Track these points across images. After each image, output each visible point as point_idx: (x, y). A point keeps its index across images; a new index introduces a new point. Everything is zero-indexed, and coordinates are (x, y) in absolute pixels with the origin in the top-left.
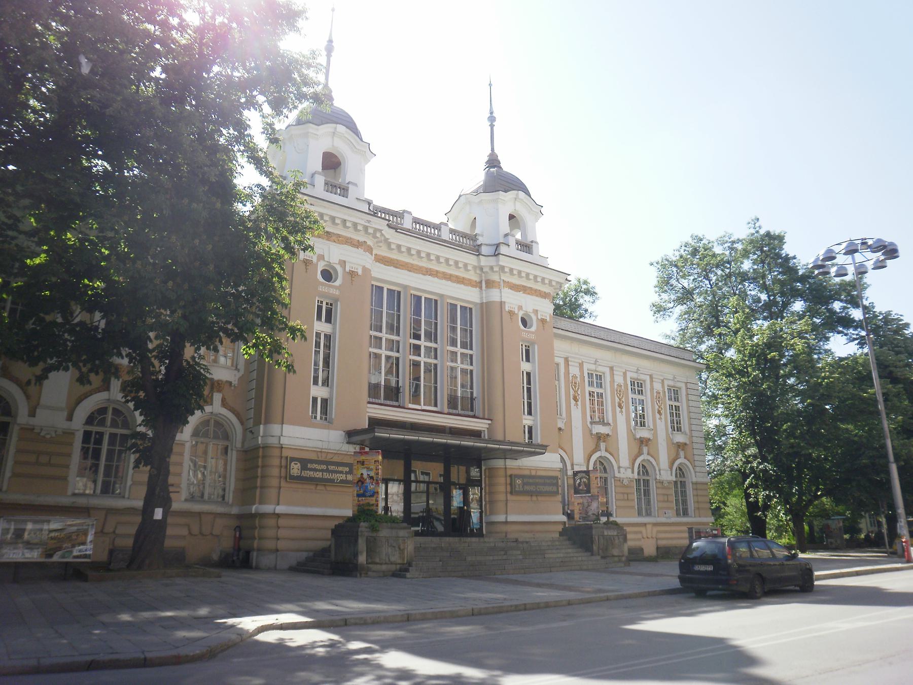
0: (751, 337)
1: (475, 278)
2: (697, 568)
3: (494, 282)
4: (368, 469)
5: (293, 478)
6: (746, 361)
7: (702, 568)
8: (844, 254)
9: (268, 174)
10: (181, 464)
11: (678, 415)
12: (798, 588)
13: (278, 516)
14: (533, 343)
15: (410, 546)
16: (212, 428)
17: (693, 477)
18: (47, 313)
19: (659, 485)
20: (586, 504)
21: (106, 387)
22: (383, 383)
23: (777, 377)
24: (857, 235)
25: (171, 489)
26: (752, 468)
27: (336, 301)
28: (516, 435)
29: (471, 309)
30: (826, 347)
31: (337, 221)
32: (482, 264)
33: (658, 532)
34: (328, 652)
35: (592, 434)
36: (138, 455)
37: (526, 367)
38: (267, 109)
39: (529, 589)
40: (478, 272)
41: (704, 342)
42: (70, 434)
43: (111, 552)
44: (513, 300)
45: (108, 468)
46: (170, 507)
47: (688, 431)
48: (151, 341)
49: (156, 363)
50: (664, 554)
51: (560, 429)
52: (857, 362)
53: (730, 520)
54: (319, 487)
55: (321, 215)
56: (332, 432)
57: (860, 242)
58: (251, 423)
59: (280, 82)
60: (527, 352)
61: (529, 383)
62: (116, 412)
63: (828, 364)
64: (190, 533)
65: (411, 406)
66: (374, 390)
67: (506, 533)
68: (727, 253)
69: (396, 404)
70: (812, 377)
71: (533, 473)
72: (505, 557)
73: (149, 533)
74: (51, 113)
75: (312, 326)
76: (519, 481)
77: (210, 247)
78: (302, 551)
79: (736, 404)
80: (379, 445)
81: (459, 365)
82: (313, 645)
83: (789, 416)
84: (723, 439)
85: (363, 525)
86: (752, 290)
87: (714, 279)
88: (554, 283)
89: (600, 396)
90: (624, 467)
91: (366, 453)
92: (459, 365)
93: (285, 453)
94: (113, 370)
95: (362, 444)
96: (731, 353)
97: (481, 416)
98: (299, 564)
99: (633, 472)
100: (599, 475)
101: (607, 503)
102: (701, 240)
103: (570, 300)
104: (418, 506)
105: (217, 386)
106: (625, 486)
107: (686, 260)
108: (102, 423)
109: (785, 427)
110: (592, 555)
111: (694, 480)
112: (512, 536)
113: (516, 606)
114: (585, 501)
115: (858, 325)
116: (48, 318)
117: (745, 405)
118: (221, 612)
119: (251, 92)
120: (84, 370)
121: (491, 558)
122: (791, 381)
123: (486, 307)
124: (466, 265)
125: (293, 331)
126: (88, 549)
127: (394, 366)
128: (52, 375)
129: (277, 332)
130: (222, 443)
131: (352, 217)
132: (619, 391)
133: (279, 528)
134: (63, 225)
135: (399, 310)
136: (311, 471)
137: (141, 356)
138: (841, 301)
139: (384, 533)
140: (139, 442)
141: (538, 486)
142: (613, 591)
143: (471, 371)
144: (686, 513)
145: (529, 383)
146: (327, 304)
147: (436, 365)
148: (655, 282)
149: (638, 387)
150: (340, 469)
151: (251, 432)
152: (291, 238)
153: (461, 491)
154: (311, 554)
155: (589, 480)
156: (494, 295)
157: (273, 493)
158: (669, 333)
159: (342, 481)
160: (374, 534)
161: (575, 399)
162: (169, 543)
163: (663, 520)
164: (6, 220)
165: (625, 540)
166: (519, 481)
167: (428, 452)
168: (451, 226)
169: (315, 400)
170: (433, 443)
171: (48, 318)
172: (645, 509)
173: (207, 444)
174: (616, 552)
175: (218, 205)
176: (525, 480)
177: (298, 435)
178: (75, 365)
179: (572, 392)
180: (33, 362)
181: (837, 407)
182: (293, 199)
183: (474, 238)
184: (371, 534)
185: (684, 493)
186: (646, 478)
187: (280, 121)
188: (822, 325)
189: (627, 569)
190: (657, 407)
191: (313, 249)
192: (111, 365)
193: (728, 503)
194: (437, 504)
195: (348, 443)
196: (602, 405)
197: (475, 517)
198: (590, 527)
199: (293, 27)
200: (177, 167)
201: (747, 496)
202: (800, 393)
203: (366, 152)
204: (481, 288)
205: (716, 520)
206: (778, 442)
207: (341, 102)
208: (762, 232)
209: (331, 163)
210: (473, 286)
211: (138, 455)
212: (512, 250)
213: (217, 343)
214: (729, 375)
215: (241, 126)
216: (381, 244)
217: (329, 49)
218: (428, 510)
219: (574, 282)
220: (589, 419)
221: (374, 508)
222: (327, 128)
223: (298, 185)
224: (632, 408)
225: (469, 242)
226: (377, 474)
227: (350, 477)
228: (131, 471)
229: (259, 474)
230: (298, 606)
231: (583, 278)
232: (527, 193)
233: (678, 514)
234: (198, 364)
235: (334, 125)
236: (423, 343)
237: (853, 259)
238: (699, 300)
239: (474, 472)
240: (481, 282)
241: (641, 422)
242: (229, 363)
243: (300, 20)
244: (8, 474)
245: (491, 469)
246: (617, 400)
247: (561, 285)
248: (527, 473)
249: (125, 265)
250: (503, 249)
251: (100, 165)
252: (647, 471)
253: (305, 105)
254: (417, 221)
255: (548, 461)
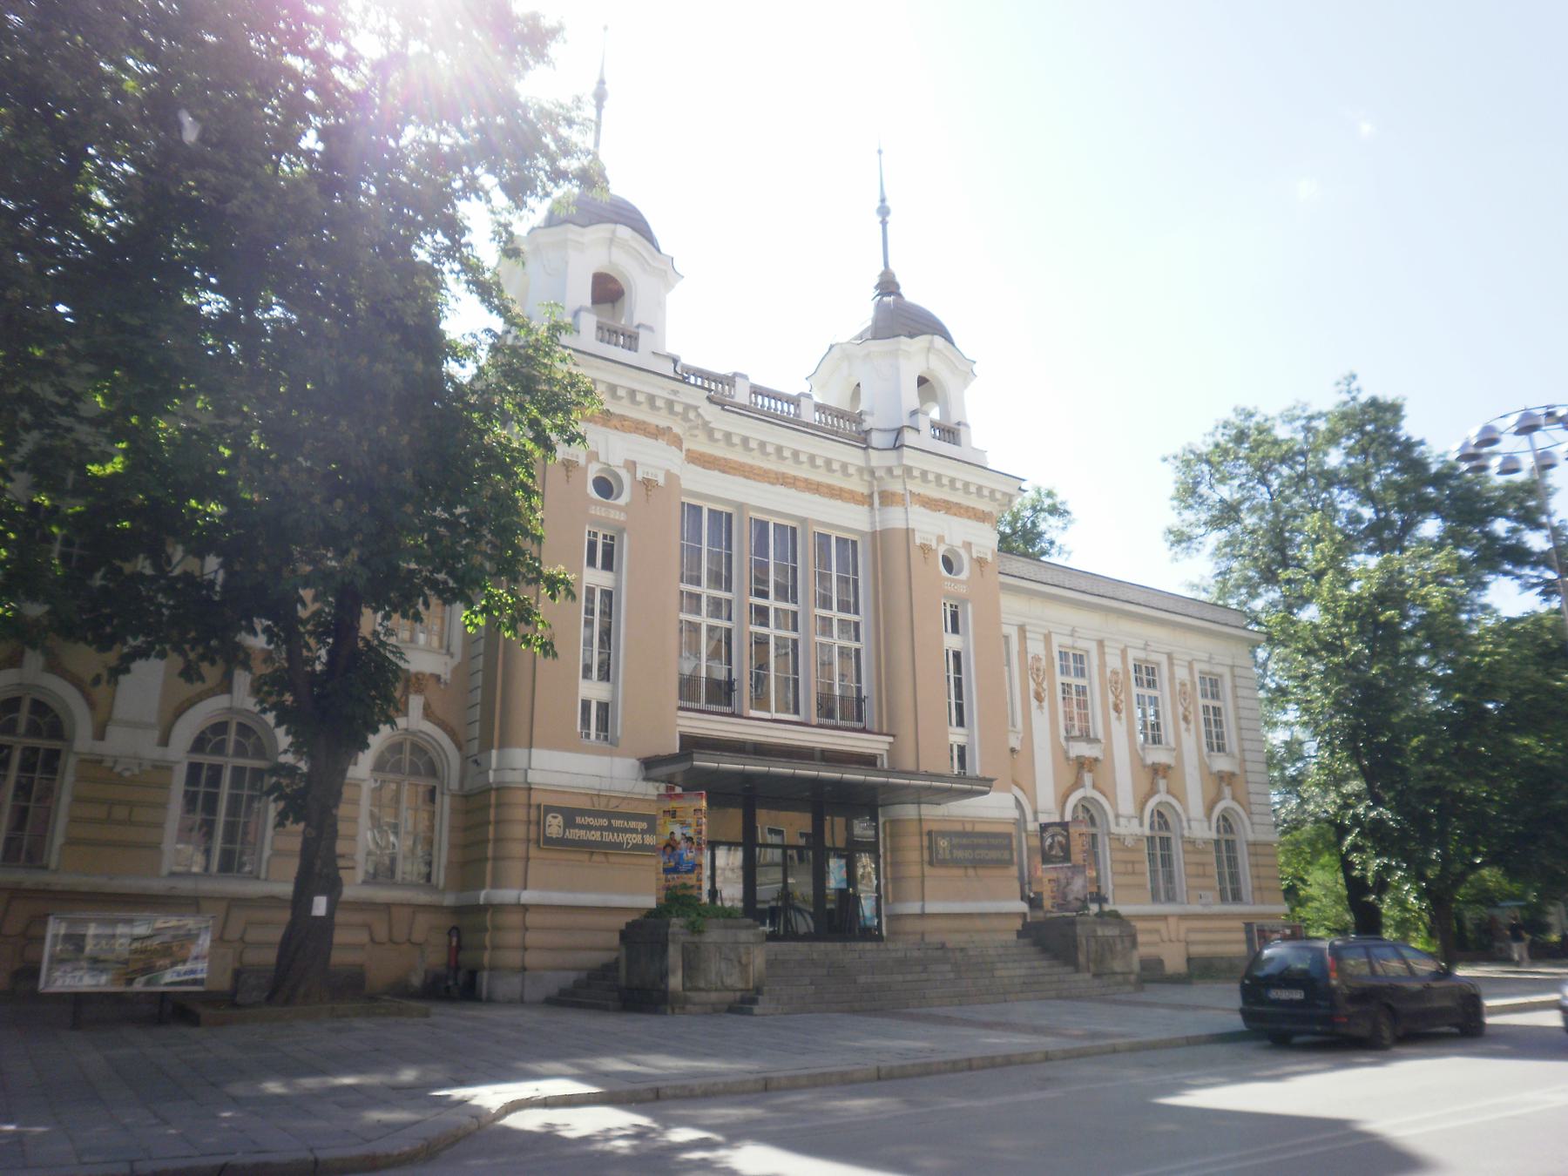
0: (1347, 585)
1: (861, 488)
2: (1275, 994)
3: (893, 494)
4: (683, 824)
5: (552, 842)
6: (1339, 627)
7: (1284, 995)
8: (1518, 433)
9: (503, 311)
10: (354, 820)
11: (1218, 723)
12: (1455, 1030)
13: (525, 908)
14: (964, 601)
15: (758, 959)
16: (407, 756)
17: (1247, 832)
18: (126, 559)
19: (1189, 848)
20: (1063, 882)
21: (226, 686)
22: (704, 674)
23: (1397, 655)
24: (1536, 403)
25: (341, 863)
26: (1355, 816)
27: (621, 531)
28: (938, 762)
29: (854, 543)
30: (1484, 600)
31: (621, 392)
32: (874, 463)
33: (1189, 930)
34: (634, 1147)
35: (1068, 758)
36: (281, 804)
37: (952, 642)
38: (500, 199)
39: (971, 1032)
40: (866, 477)
41: (1259, 595)
42: (165, 768)
43: (237, 974)
44: (928, 527)
45: (231, 829)
46: (340, 893)
47: (1236, 751)
48: (304, 605)
49: (312, 642)
50: (1202, 969)
51: (1013, 750)
52: (1542, 627)
53: (1318, 910)
54: (596, 858)
55: (594, 382)
56: (617, 760)
57: (1543, 411)
58: (475, 747)
59: (518, 150)
60: (955, 616)
61: (958, 669)
62: (244, 730)
63: (1489, 630)
64: (372, 940)
65: (753, 713)
66: (688, 687)
67: (923, 934)
68: (1300, 436)
69: (727, 709)
70: (1461, 653)
71: (969, 828)
72: (924, 976)
73: (305, 940)
74: (131, 213)
75: (580, 579)
76: (943, 843)
77: (405, 439)
78: (564, 969)
79: (1320, 700)
80: (698, 782)
81: (837, 641)
82: (606, 1135)
83: (1421, 724)
84: (1299, 765)
85: (676, 923)
86: (1346, 501)
87: (1276, 484)
88: (998, 496)
89: (1082, 691)
90: (1125, 816)
91: (678, 796)
92: (837, 641)
93: (536, 798)
94: (241, 656)
95: (670, 781)
96: (1310, 614)
97: (876, 728)
98: (563, 992)
99: (1141, 824)
100: (1084, 829)
101: (1098, 879)
102: (1251, 415)
103: (1024, 525)
104: (768, 888)
105: (417, 682)
106: (1127, 849)
107: (1226, 452)
108: (219, 749)
109: (1415, 742)
110: (1077, 970)
111: (1251, 837)
112: (934, 939)
113: (954, 1062)
114: (1062, 876)
115: (1542, 560)
116: (128, 568)
117: (1339, 706)
118: (438, 1077)
119: (472, 169)
120: (192, 656)
121: (900, 978)
122: (1422, 661)
123: (880, 539)
124: (844, 466)
125: (552, 583)
126: (201, 969)
127: (723, 645)
128: (139, 666)
129: (523, 584)
130: (424, 783)
131: (644, 385)
132: (1114, 684)
133: (526, 929)
134: (152, 404)
135: (729, 547)
136: (584, 830)
137: (286, 629)
138: (1508, 517)
139: (714, 935)
140: (284, 782)
141: (983, 850)
142: (1122, 1036)
143: (858, 651)
144: (1237, 897)
145: (958, 669)
146: (605, 537)
147: (795, 642)
148: (1171, 490)
149: (1147, 674)
150: (632, 824)
151: (476, 761)
152: (546, 422)
153: (843, 862)
154: (583, 975)
155: (1067, 837)
156: (895, 518)
157: (515, 868)
158: (1196, 580)
159: (636, 847)
160: (696, 939)
161: (1039, 698)
162: (338, 957)
163: (1196, 908)
164: (57, 399)
165: (1134, 944)
166: (943, 843)
167: (784, 794)
168: (818, 399)
169: (586, 705)
170: (793, 777)
171: (128, 568)
172: (1164, 889)
173: (399, 784)
174: (1118, 966)
175: (419, 366)
176: (955, 841)
177: (558, 767)
178: (177, 648)
179: (1032, 685)
180: (104, 644)
181: (1507, 707)
182: (547, 354)
183: (857, 419)
184: (689, 939)
185: (1233, 861)
186: (1165, 834)
187: (521, 218)
188: (1475, 560)
189: (1143, 997)
190: (1181, 710)
191: (584, 440)
192: (239, 647)
193: (1310, 880)
194: (801, 883)
195: (647, 779)
196: (1085, 707)
197: (867, 906)
198: (1071, 923)
199: (540, 56)
200: (347, 301)
201: (1347, 866)
202: (1437, 683)
203: (666, 273)
204: (871, 505)
205: (1292, 910)
206: (1403, 771)
207: (621, 187)
208: (1363, 398)
209: (607, 291)
210: (857, 502)
211: (281, 804)
212: (926, 438)
213: (421, 607)
214: (1308, 652)
215: (454, 228)
216: (696, 432)
217: (600, 97)
218: (786, 894)
219: (1031, 494)
220: (1063, 733)
221: (695, 892)
222: (600, 231)
223: (556, 328)
224: (1139, 713)
225: (848, 426)
226: (700, 832)
227: (650, 840)
228: (269, 832)
229: (491, 836)
230: (573, 1065)
231: (1045, 486)
232: (948, 338)
233: (1223, 899)
234: (383, 644)
235: (611, 226)
236: (772, 603)
237: (1531, 442)
238: (1250, 521)
239: (862, 829)
240: (871, 496)
241: (1154, 735)
242: (435, 642)
243: (553, 44)
244: (59, 839)
245: (894, 822)
246: (1111, 698)
247: (1010, 498)
248: (958, 827)
249: (261, 472)
250: (909, 438)
251: (212, 304)
252: (1166, 823)
253: (569, 189)
254: (757, 391)
255: (994, 807)
